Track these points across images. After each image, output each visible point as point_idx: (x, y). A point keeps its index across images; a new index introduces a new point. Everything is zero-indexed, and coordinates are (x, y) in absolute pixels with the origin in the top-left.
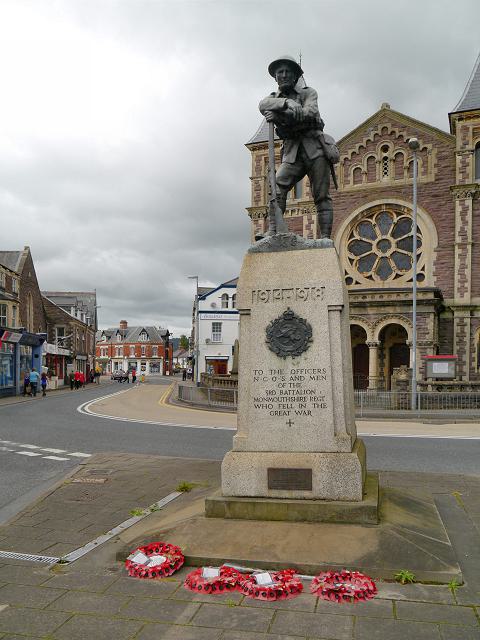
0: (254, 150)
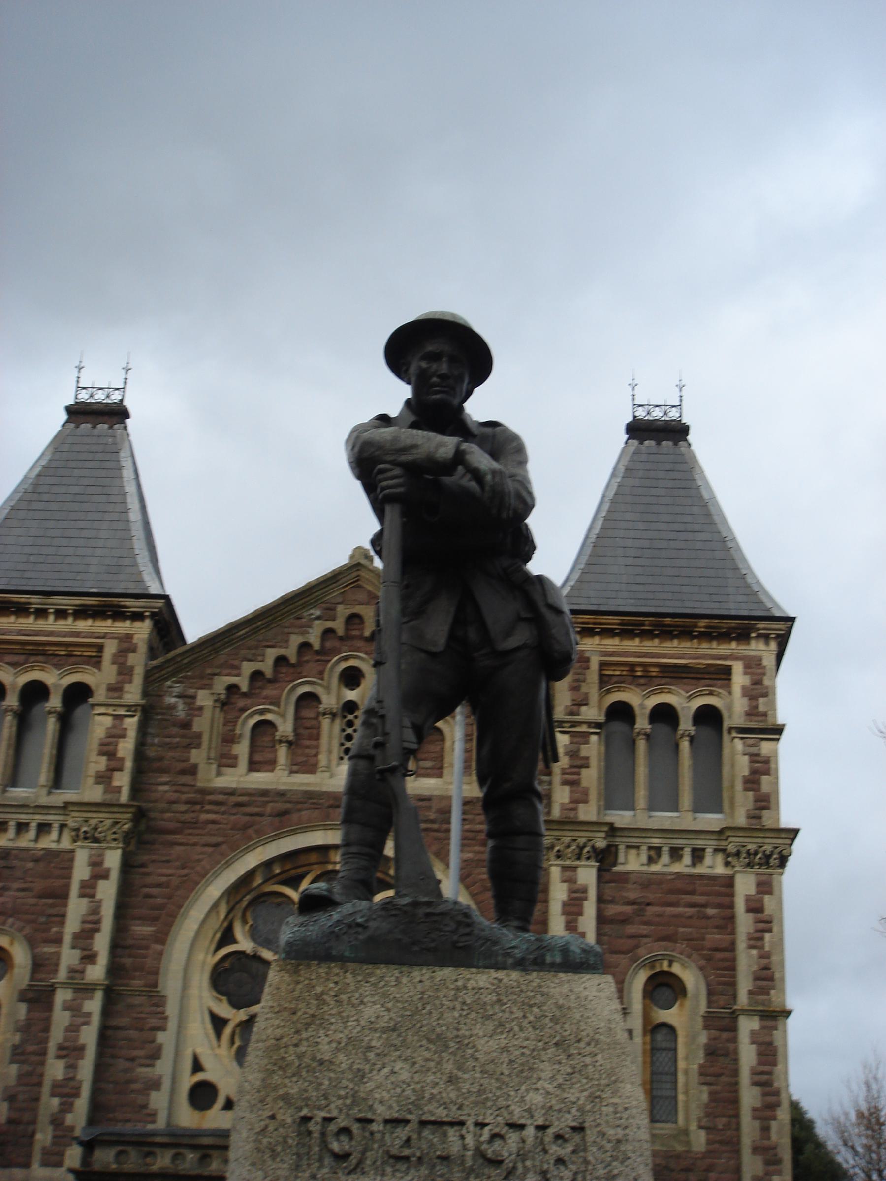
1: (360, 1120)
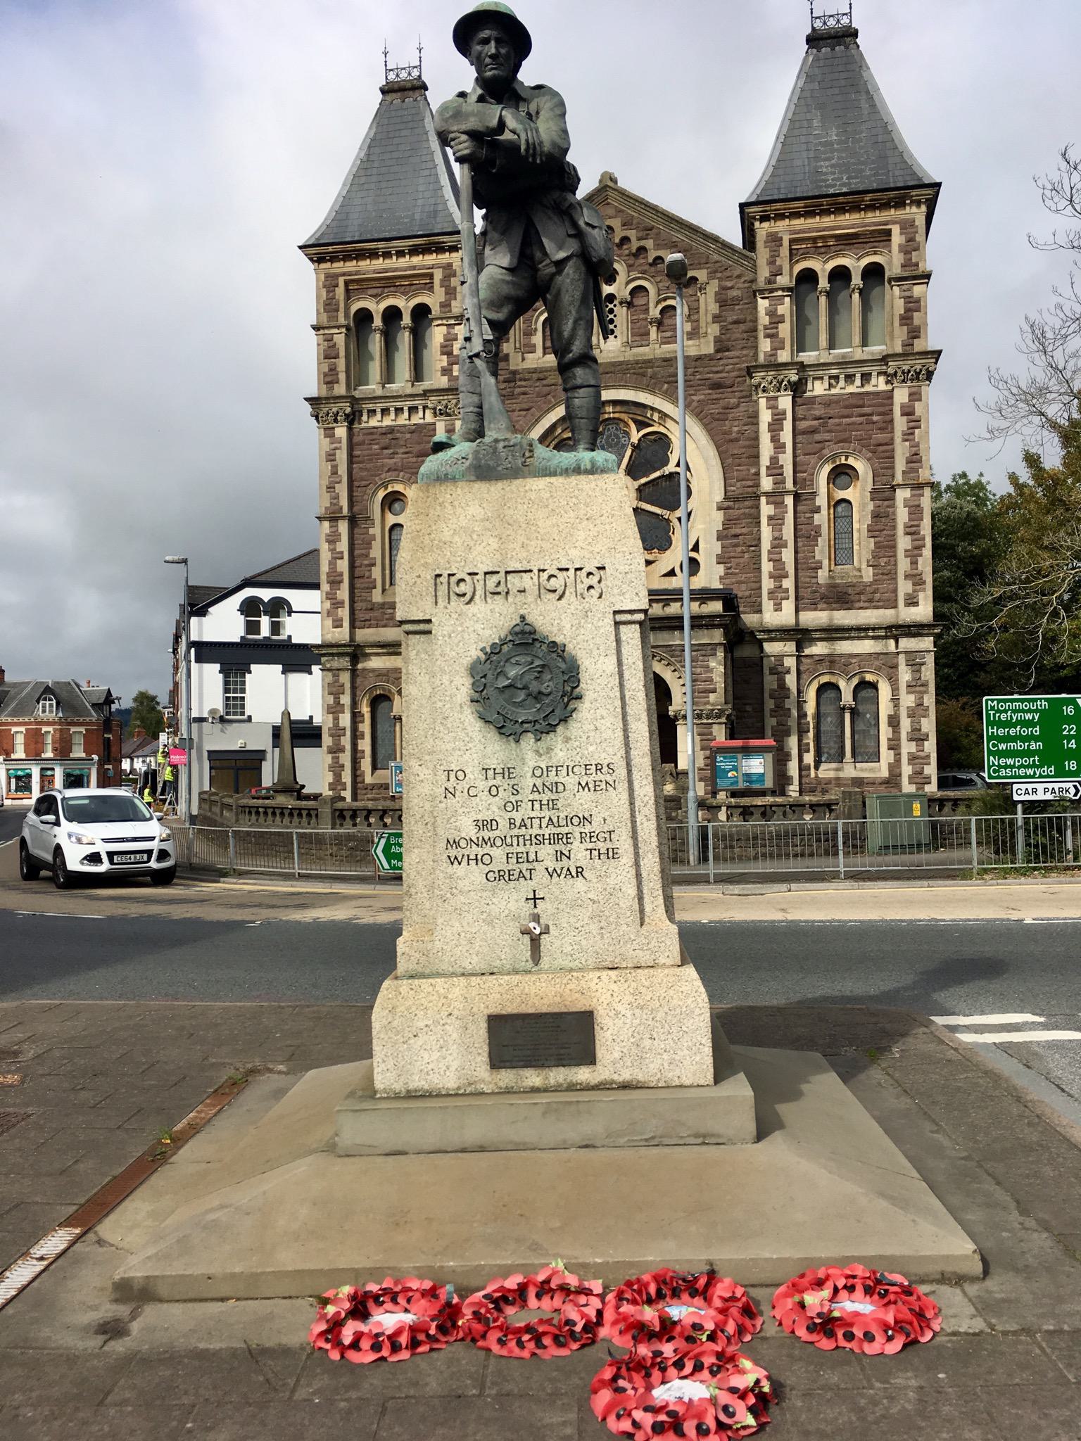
0: (318, 259)
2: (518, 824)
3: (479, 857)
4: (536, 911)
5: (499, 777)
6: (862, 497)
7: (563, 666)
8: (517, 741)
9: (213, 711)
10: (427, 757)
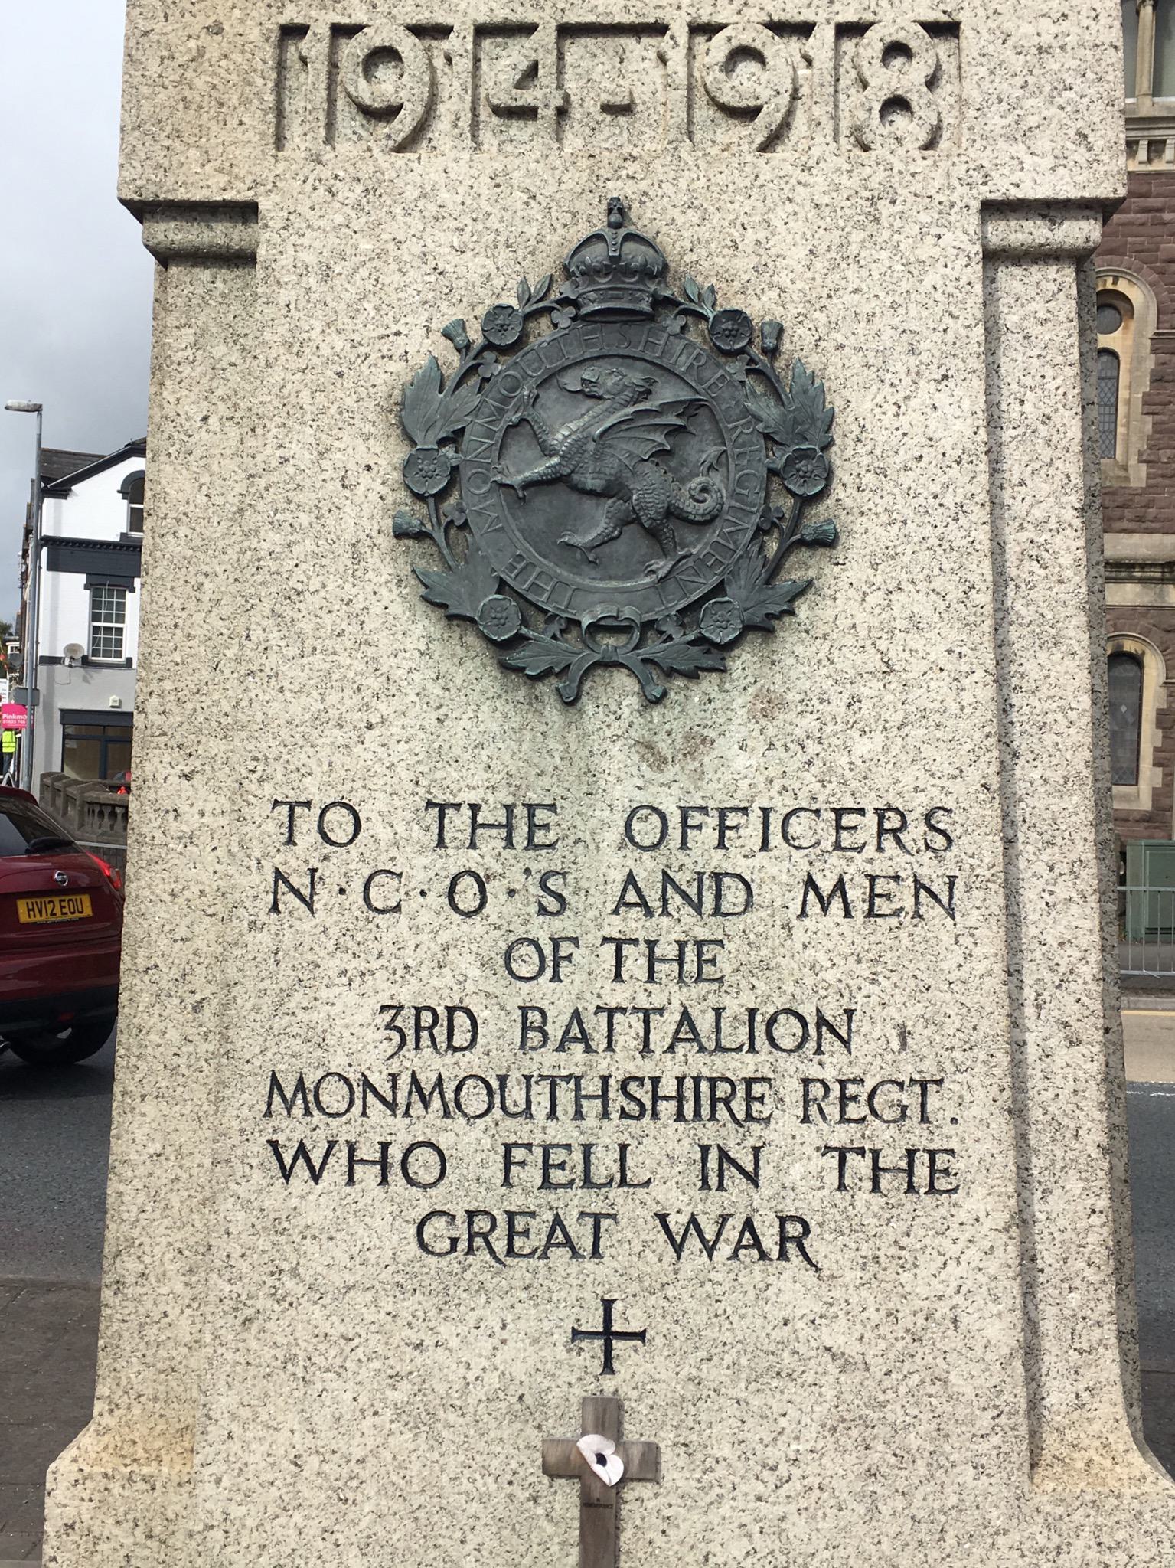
1: (419, 31)
2: (555, 1032)
3: (395, 1153)
4: (609, 1384)
5: (491, 842)
6: (1137, 345)
7: (769, 411)
8: (571, 702)
9: (72, 648)
10: (216, 747)
